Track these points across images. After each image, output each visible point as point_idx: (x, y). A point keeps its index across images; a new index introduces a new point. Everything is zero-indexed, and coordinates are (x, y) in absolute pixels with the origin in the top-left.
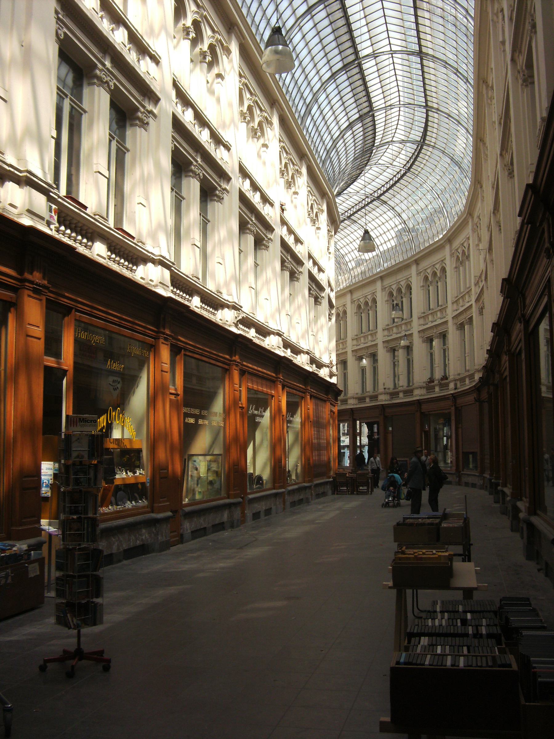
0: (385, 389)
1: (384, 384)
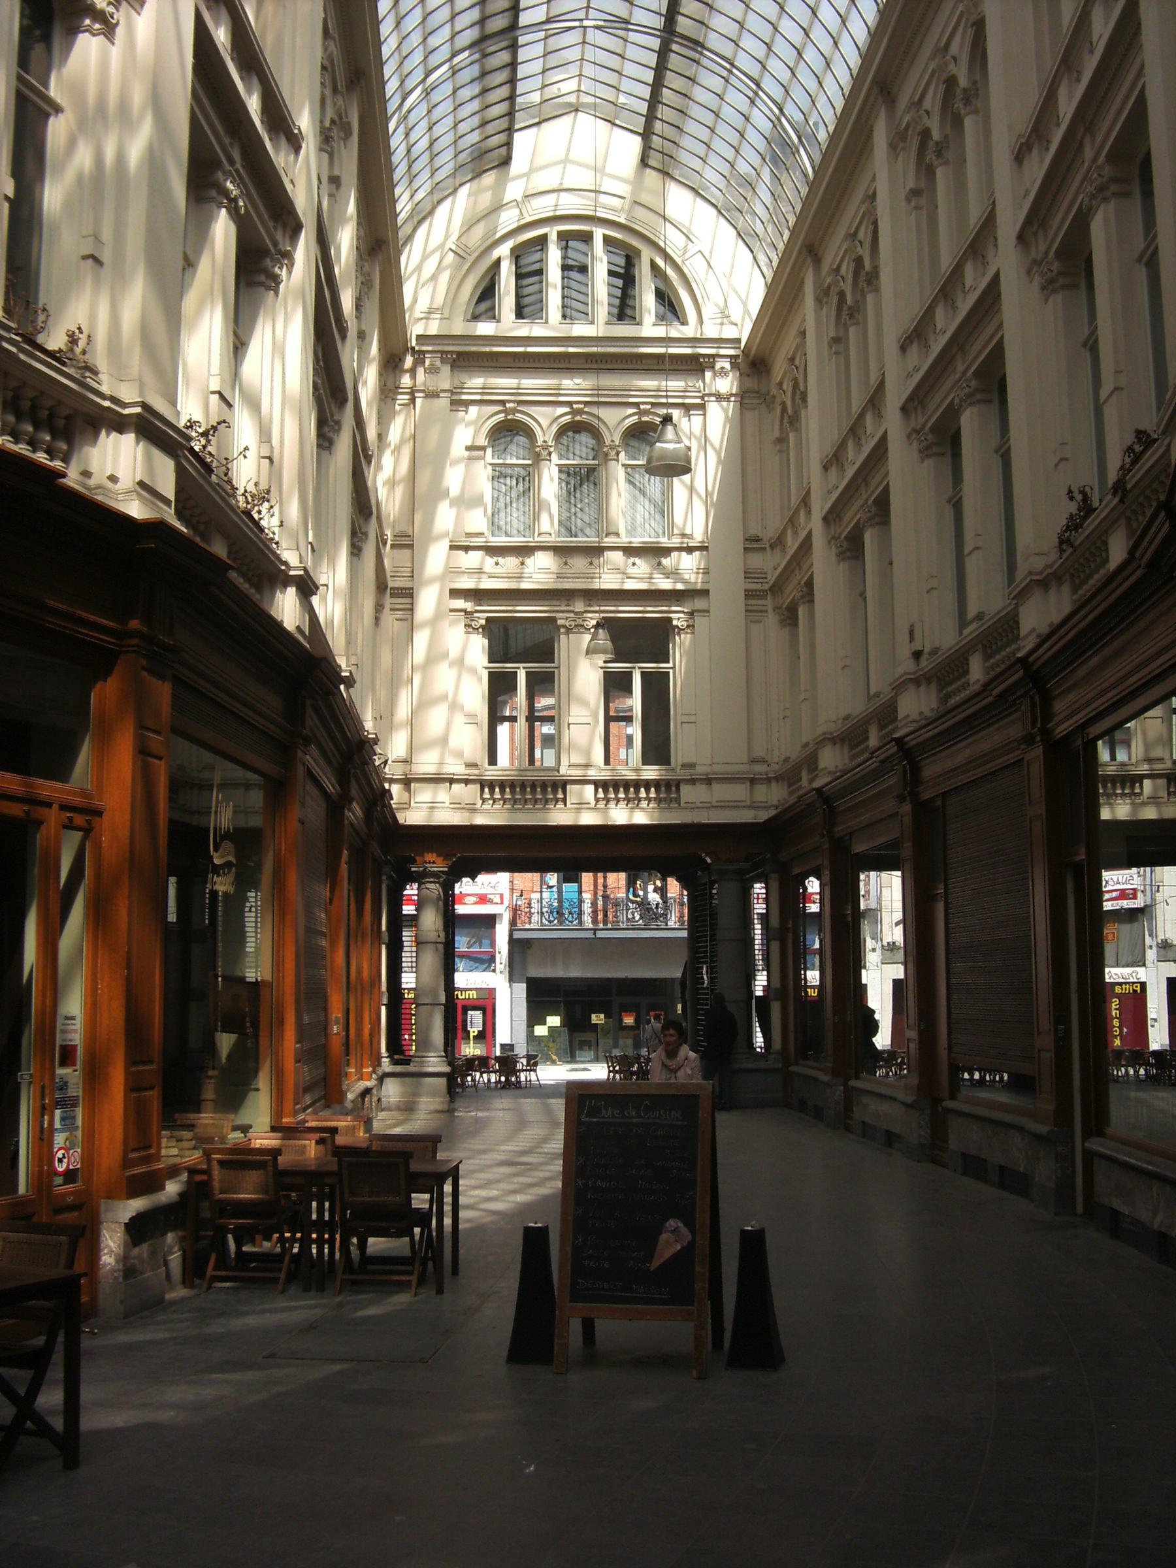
0: (917, 655)
1: (911, 632)
